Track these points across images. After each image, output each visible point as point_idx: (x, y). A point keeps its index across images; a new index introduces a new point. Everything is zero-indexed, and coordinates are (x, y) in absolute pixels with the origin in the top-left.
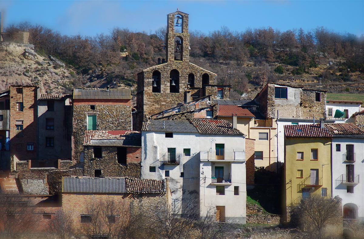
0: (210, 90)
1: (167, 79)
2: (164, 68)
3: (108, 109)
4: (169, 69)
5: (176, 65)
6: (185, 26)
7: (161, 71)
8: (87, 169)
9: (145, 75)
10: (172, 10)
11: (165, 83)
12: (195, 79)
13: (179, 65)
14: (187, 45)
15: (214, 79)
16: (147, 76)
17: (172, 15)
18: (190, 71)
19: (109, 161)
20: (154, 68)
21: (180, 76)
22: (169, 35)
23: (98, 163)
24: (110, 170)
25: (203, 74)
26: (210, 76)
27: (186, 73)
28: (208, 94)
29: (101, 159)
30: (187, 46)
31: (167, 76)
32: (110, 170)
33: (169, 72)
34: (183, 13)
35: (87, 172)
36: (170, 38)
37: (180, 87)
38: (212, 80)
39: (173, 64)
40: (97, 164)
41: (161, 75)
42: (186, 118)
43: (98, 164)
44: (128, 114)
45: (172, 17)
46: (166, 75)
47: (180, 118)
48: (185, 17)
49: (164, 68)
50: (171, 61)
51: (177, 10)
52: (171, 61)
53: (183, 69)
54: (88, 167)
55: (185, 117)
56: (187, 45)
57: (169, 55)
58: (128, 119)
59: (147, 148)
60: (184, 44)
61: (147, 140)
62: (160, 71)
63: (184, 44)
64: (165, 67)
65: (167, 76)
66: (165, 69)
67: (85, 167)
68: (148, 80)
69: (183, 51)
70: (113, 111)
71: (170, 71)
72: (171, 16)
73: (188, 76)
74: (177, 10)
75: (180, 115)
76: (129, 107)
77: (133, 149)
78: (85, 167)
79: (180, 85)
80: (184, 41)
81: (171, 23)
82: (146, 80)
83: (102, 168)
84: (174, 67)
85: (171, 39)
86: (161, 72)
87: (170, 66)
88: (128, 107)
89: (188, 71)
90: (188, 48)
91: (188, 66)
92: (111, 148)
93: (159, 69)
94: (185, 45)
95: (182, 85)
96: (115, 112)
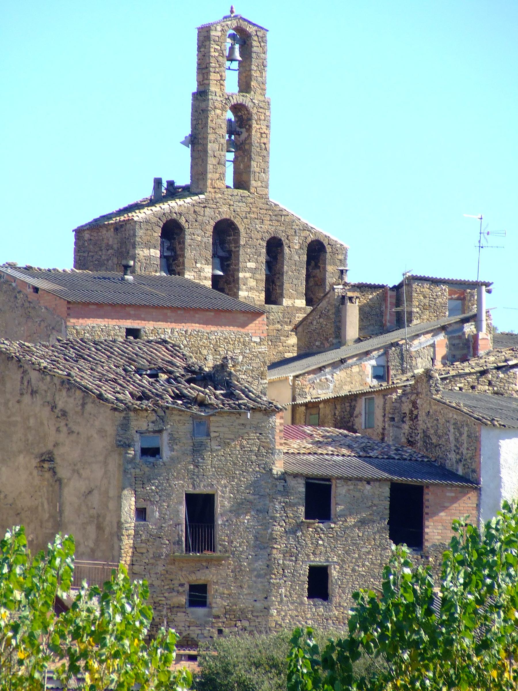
0: (425, 297)
1: (204, 252)
2: (195, 212)
3: (185, 342)
4: (210, 218)
5: (232, 203)
6: (255, 68)
7: (187, 221)
8: (281, 562)
9: (140, 233)
10: (213, 14)
11: (198, 265)
12: (286, 257)
13: (240, 204)
14: (264, 135)
15: (340, 260)
16: (146, 238)
17: (219, 28)
18: (272, 229)
19: (361, 535)
20: (167, 210)
21: (242, 242)
22: (210, 97)
23: (323, 540)
24: (363, 566)
25: (309, 240)
26: (329, 249)
27: (259, 236)
28: (418, 309)
29: (333, 525)
30: (262, 141)
31: (205, 240)
32: (363, 566)
33: (210, 229)
34: (249, 22)
35: (281, 572)
36: (215, 108)
37: (240, 281)
38: (334, 264)
39: (221, 201)
40: (318, 544)
41: (188, 237)
42: (491, 388)
43: (320, 542)
44: (254, 365)
45: (219, 34)
46: (199, 239)
47: (473, 387)
48: (256, 38)
49: (195, 212)
50: (217, 191)
51: (232, 12)
52: (217, 191)
53: (251, 218)
54: (287, 553)
55: (490, 384)
56: (264, 135)
57: (211, 166)
58: (256, 382)
59: (502, 490)
60: (253, 132)
61: (502, 461)
62: (182, 221)
63: (256, 131)
64: (197, 209)
65: (205, 240)
66: (200, 218)
67: (275, 551)
68: (146, 252)
69: (253, 156)
70: (205, 352)
71: (213, 223)
72: (216, 30)
73: (265, 244)
74: (232, 12)
75: (474, 377)
76: (258, 340)
77: (448, 494)
78: (275, 551)
79: (241, 275)
80: (254, 122)
81: (217, 54)
82: (141, 253)
83: (335, 559)
84: (225, 212)
85: (218, 112)
86: (186, 225)
87: (214, 206)
88: (254, 339)
89: (265, 227)
90: (266, 149)
91: (265, 212)
92: (368, 487)
93: (180, 214)
94: (259, 135)
95: (248, 275)
96: (210, 357)
